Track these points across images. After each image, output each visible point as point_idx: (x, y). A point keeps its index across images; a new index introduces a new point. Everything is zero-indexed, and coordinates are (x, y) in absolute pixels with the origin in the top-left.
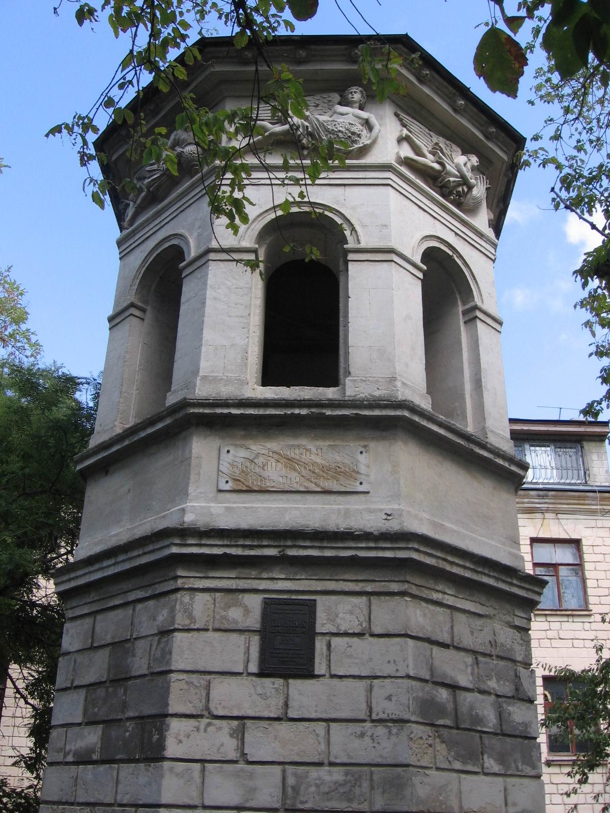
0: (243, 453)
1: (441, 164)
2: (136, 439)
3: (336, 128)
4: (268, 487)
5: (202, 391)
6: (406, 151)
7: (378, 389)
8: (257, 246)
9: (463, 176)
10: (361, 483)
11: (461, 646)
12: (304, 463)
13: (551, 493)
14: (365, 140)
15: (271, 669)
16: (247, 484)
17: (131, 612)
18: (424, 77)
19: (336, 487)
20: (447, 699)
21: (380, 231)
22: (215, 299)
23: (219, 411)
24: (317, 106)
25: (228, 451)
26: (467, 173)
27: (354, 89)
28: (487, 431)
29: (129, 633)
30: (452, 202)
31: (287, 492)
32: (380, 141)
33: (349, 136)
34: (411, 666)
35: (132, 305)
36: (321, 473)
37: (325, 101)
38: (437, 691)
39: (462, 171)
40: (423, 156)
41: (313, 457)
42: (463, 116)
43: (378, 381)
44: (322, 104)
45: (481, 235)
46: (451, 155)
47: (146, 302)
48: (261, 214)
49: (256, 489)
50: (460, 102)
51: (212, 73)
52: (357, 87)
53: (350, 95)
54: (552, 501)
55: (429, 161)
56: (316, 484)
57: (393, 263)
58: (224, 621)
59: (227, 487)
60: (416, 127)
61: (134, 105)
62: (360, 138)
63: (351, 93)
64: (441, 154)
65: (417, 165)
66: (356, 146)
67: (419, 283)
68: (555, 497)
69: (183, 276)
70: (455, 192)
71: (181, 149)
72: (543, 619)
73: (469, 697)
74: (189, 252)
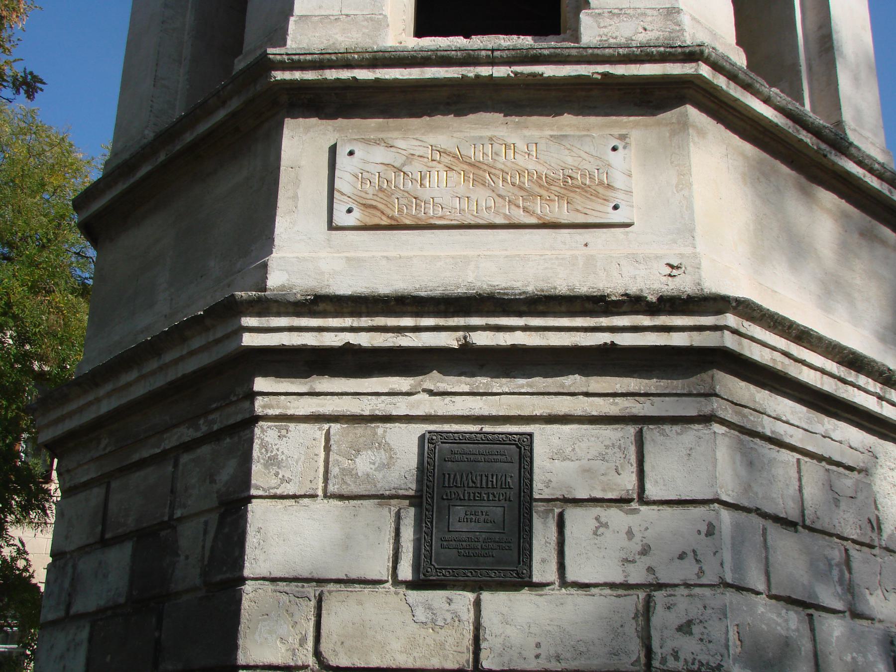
0: (380, 155)
2: (178, 147)
7: (645, 30)
11: (818, 526)
12: (503, 171)
16: (390, 213)
17: (170, 469)
19: (566, 216)
23: (331, 74)
29: (167, 510)
34: (728, 566)
36: (537, 189)
41: (521, 161)
49: (408, 222)
56: (525, 210)
58: (348, 479)
61: (423, 580)
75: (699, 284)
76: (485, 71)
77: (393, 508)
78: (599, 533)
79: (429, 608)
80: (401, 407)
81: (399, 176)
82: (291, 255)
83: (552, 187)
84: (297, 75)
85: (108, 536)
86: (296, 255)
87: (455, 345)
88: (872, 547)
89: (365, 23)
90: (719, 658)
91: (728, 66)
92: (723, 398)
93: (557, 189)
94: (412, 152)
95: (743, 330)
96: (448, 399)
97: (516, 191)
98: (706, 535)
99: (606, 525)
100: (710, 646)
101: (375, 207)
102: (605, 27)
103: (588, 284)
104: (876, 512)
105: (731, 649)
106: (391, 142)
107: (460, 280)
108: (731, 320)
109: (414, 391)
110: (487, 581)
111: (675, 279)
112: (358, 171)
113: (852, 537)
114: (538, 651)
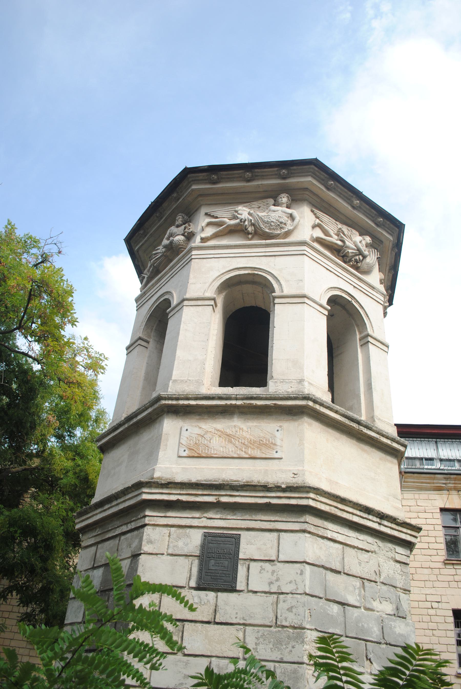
0: (197, 431)
1: (343, 241)
3: (270, 220)
4: (212, 454)
5: (173, 389)
6: (318, 233)
7: (291, 387)
8: (215, 296)
9: (359, 250)
10: (277, 452)
12: (238, 438)
13: (452, 476)
14: (289, 227)
15: (205, 584)
17: (118, 541)
18: (330, 186)
19: (259, 454)
20: (337, 613)
21: (298, 284)
22: (186, 330)
24: (259, 207)
25: (187, 430)
26: (361, 248)
27: (283, 195)
28: (375, 418)
30: (352, 266)
31: (225, 458)
32: (300, 227)
33: (278, 225)
35: (140, 338)
36: (249, 445)
37: (265, 204)
38: (329, 606)
39: (358, 246)
40: (330, 236)
41: (244, 434)
42: (359, 211)
43: (292, 382)
44: (263, 206)
45: (373, 288)
46: (350, 235)
47: (149, 336)
48: (219, 276)
49: (204, 455)
50: (356, 202)
51: (193, 190)
52: (285, 194)
53: (280, 199)
54: (453, 482)
55: (334, 239)
56: (245, 452)
57: (305, 304)
59: (185, 454)
60: (326, 219)
62: (286, 225)
63: (281, 198)
64: (342, 235)
65: (326, 242)
66: (283, 231)
67: (325, 318)
68: (455, 479)
69: (169, 317)
70: (353, 260)
71: (172, 239)
72: (452, 567)
73: (355, 613)
74: (173, 302)
75: (304, 481)
76: (234, 402)
77: (190, 560)
78: (261, 572)
79: (199, 597)
80: (195, 523)
81: (202, 439)
82: (163, 466)
83: (255, 444)
84: (170, 402)
85: (95, 566)
86: (165, 466)
87: (215, 501)
88: (376, 582)
89: (196, 383)
90: (302, 621)
91: (319, 401)
92: (310, 524)
93: (256, 445)
94: (207, 430)
95: (317, 499)
96: (212, 520)
97: (242, 445)
98: (300, 575)
99: (264, 569)
100: (299, 617)
101: (193, 450)
102: (278, 386)
103: (265, 480)
104: (379, 568)
105: (306, 618)
106: (200, 426)
107: (220, 477)
108: (312, 495)
109: (200, 517)
110: (220, 588)
111: (295, 479)
112: (188, 436)
113: (366, 578)
114: (236, 616)
